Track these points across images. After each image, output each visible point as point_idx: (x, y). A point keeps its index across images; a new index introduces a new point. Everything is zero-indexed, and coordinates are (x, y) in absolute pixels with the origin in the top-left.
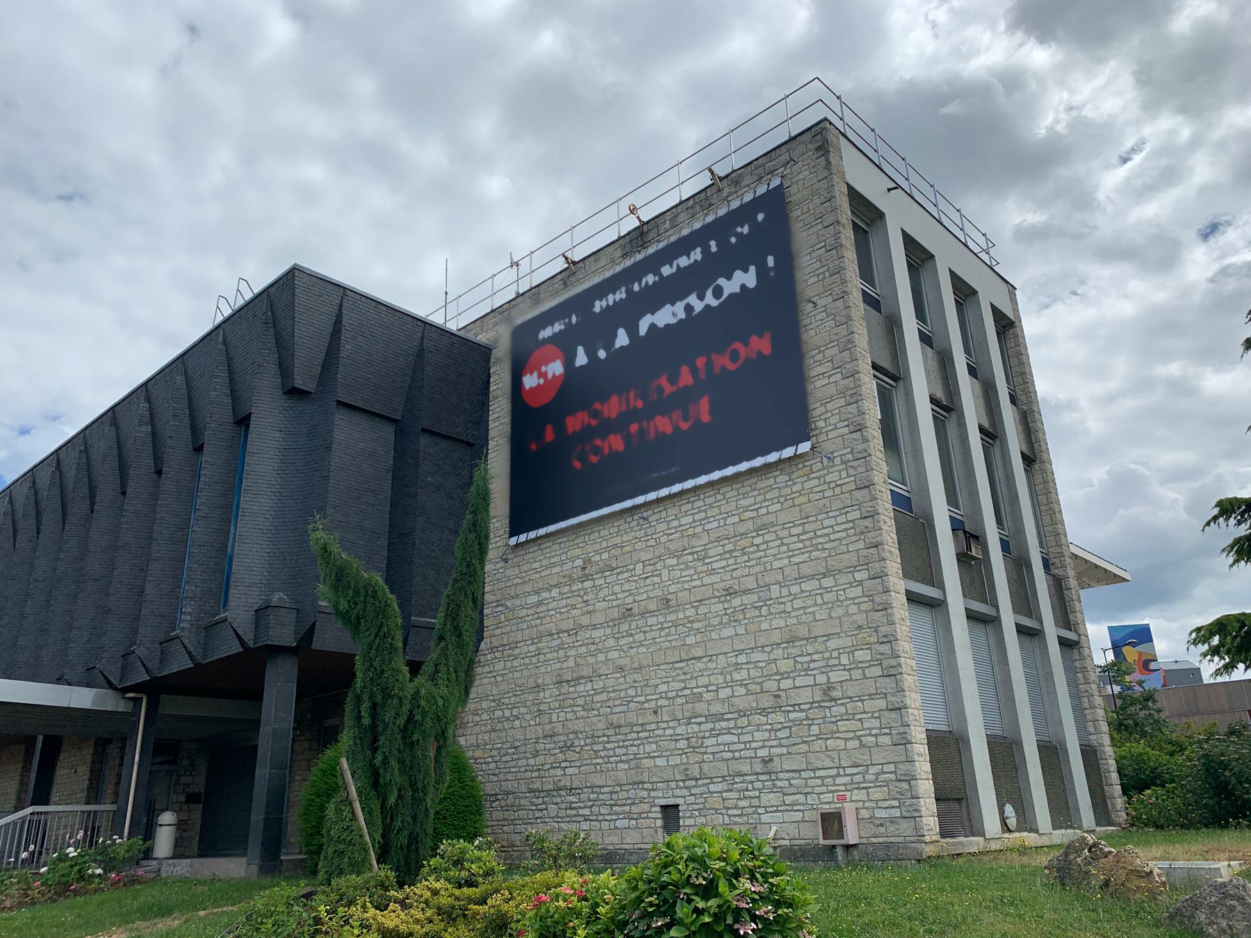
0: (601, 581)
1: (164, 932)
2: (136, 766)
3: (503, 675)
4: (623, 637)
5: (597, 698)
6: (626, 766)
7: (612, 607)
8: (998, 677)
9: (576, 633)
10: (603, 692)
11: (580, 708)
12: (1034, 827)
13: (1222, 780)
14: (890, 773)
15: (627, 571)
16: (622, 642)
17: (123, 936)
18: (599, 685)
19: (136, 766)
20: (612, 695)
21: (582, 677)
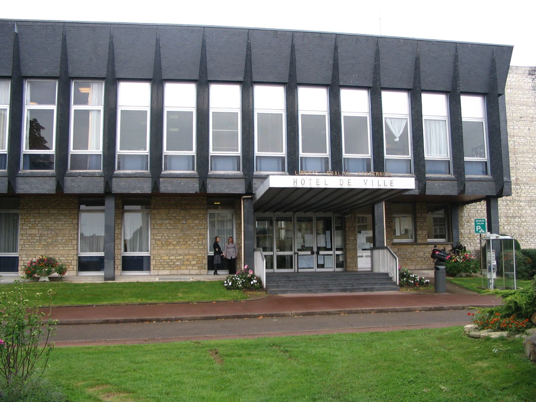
0: (523, 187)
1: (275, 390)
2: (385, 230)
3: (481, 211)
4: (532, 206)
5: (522, 224)
6: (534, 245)
7: (528, 196)
8: (451, 232)
9: (513, 202)
10: (525, 222)
11: (516, 226)
12: (341, 263)
13: (223, 256)
14: (23, 257)
15: (533, 186)
16: (532, 208)
17: (509, 399)
18: (523, 220)
19: (385, 230)
20: (528, 223)
21: (517, 216)
